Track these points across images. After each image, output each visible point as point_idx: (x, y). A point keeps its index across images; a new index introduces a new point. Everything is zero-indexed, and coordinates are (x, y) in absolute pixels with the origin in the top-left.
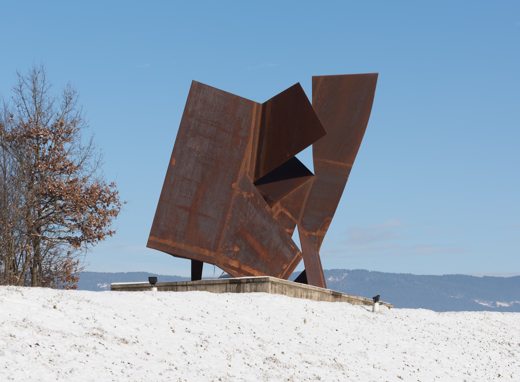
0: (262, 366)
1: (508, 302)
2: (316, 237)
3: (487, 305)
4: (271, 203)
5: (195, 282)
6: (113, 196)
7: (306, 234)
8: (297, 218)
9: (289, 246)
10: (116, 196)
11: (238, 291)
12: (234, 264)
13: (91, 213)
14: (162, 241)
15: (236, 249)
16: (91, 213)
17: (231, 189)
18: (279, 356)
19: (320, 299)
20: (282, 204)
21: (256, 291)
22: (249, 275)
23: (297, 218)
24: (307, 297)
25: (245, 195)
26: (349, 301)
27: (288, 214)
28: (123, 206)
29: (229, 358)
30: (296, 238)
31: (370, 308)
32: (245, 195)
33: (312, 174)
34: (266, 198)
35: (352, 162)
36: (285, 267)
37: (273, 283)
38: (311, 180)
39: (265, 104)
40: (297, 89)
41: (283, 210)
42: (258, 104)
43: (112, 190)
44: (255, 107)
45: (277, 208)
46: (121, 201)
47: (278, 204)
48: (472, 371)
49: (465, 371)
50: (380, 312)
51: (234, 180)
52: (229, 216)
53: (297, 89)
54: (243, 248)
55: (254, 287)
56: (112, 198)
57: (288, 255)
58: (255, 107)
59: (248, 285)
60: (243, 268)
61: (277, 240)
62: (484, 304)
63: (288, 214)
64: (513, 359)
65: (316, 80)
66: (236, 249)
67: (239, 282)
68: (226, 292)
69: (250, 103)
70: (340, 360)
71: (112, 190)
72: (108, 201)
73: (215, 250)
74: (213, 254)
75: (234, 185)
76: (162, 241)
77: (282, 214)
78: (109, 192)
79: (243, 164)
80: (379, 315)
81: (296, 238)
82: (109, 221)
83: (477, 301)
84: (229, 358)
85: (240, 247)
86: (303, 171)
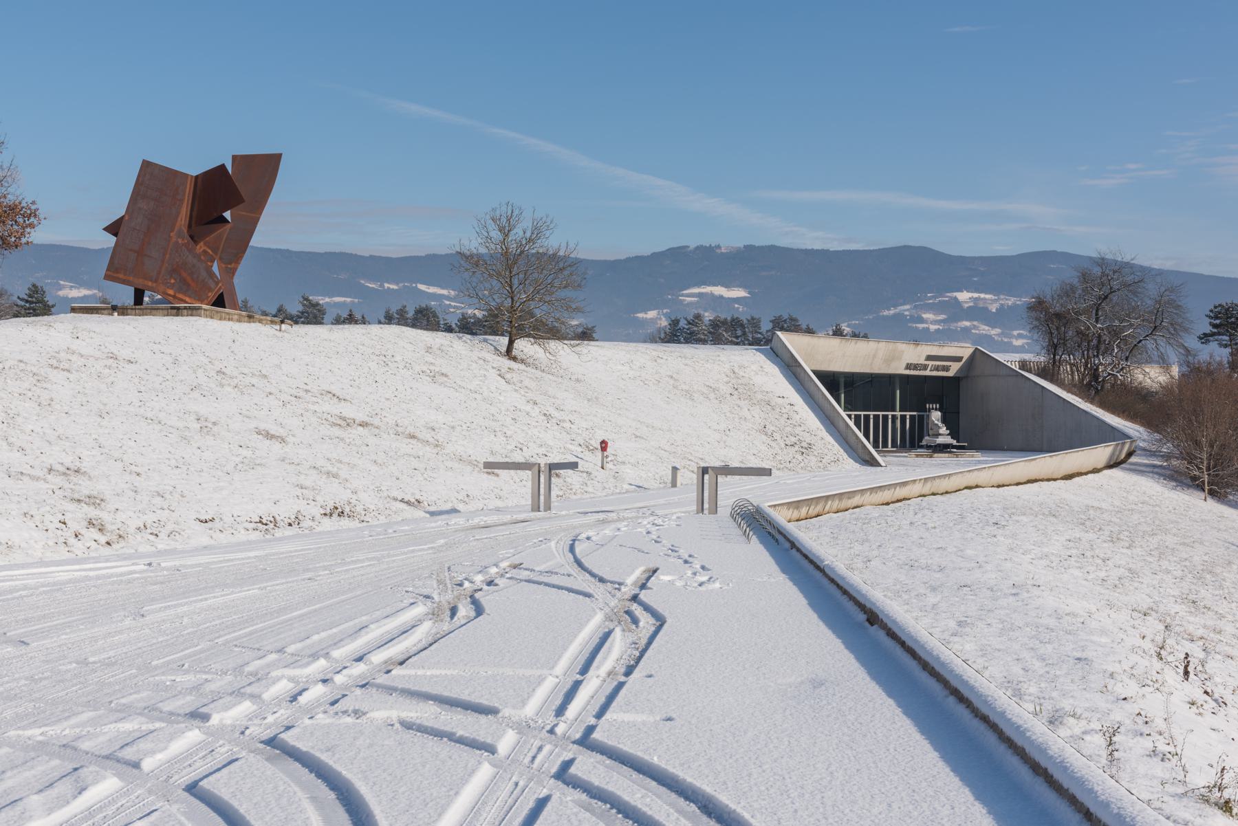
0: (216, 377)
1: (397, 284)
2: (231, 269)
3: (373, 286)
4: (196, 242)
5: (137, 307)
6: (35, 213)
7: (224, 266)
8: (216, 254)
9: (213, 279)
10: (37, 213)
11: (177, 315)
12: (171, 292)
13: (12, 225)
14: (115, 275)
15: (173, 281)
16: (12, 225)
17: (170, 236)
18: (224, 370)
19: (239, 321)
20: (205, 244)
21: (192, 315)
22: (187, 303)
23: (216, 254)
24: (229, 319)
25: (180, 241)
26: (260, 321)
27: (209, 251)
28: (43, 222)
29: (195, 372)
30: (215, 268)
31: (278, 327)
32: (180, 241)
33: (228, 222)
34: (192, 237)
35: (261, 214)
36: (210, 294)
37: (205, 310)
38: (228, 226)
39: (197, 177)
40: (223, 167)
41: (205, 248)
42: (192, 176)
43: (33, 207)
44: (189, 178)
45: (201, 247)
46: (42, 216)
47: (202, 244)
48: (356, 378)
49: (351, 378)
50: (285, 331)
51: (172, 231)
52: (168, 256)
53: (223, 167)
54: (178, 280)
55: (190, 312)
56: (34, 214)
57: (213, 286)
58: (189, 178)
59: (185, 311)
60: (177, 295)
61: (204, 274)
62: (370, 286)
63: (209, 251)
64: (387, 369)
65: (234, 158)
66: (173, 281)
67: (178, 309)
68: (168, 315)
69: (187, 175)
70: (264, 372)
71: (33, 207)
72: (29, 217)
73: (156, 281)
74: (154, 285)
75: (172, 234)
76: (115, 275)
77: (205, 251)
78: (30, 209)
79: (179, 219)
80: (285, 334)
81: (215, 268)
82: (29, 233)
83: (363, 282)
84: (195, 372)
85: (175, 280)
86: (226, 221)
